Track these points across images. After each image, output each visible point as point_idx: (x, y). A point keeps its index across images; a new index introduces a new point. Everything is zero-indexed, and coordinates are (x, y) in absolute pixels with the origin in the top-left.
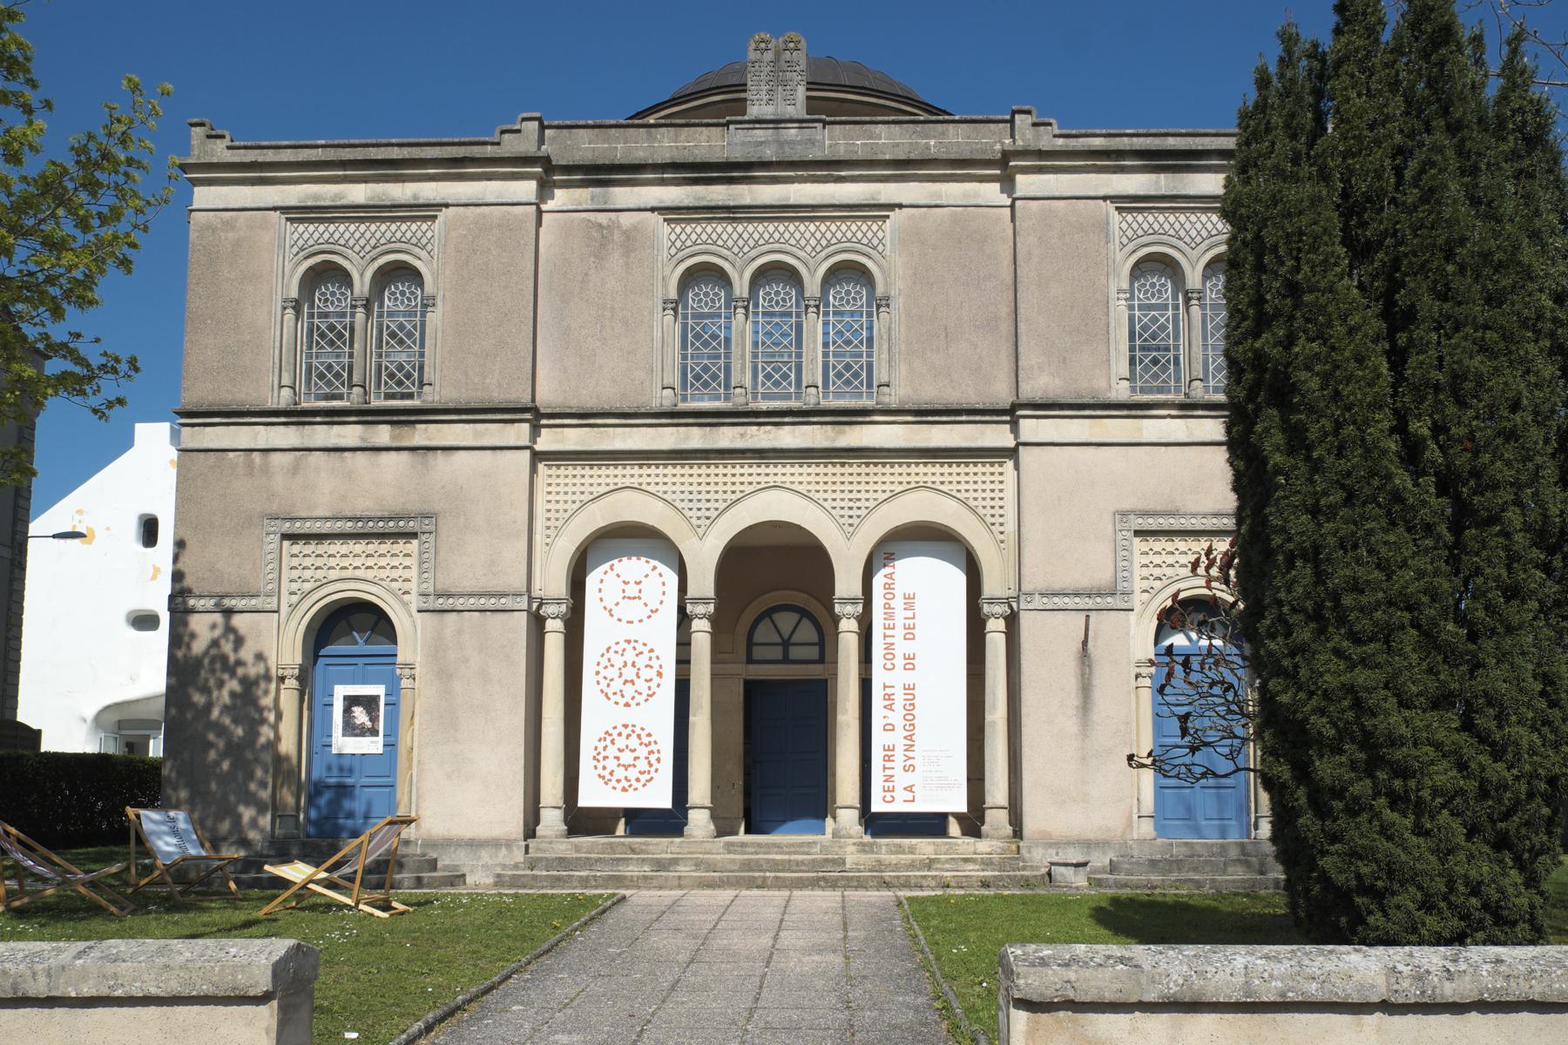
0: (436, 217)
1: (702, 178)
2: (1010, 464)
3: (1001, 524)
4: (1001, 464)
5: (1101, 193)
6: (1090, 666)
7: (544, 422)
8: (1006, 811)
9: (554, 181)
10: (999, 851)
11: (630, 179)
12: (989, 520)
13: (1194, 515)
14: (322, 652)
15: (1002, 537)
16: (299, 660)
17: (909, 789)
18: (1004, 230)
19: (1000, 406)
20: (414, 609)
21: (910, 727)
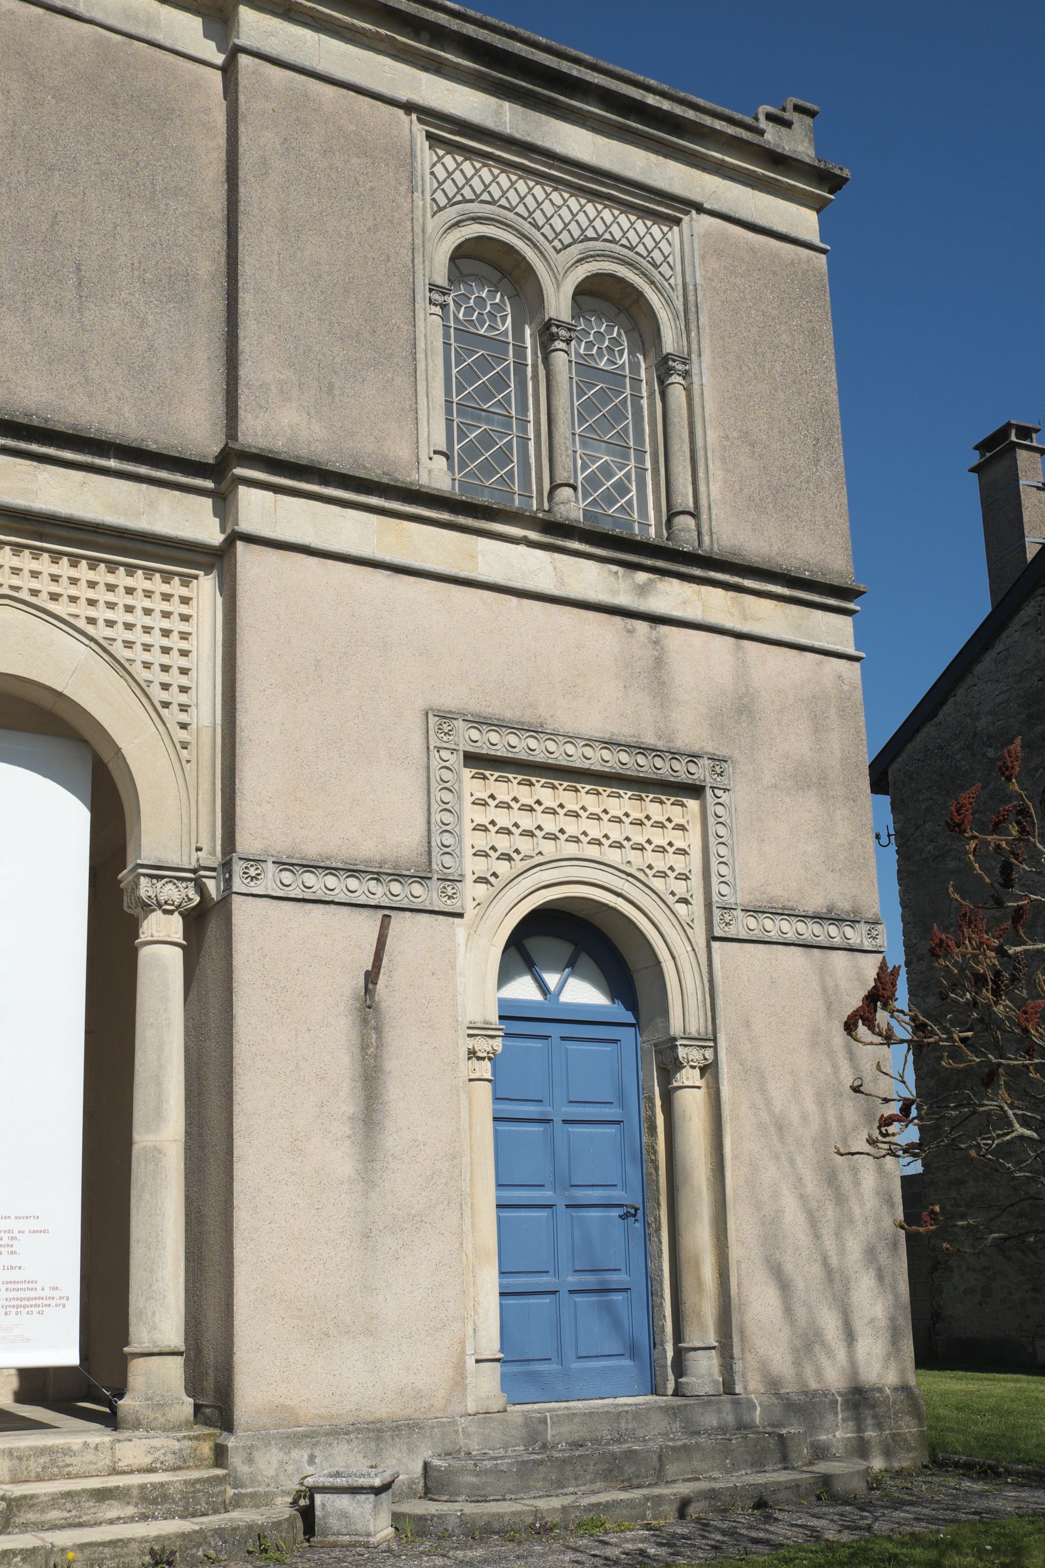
2: (206, 586)
3: (184, 708)
4: (186, 580)
5: (403, 95)
6: (378, 1029)
8: (180, 1360)
10: (171, 1460)
12: (158, 695)
13: (571, 738)
15: (183, 735)
18: (207, 111)
19: (192, 453)
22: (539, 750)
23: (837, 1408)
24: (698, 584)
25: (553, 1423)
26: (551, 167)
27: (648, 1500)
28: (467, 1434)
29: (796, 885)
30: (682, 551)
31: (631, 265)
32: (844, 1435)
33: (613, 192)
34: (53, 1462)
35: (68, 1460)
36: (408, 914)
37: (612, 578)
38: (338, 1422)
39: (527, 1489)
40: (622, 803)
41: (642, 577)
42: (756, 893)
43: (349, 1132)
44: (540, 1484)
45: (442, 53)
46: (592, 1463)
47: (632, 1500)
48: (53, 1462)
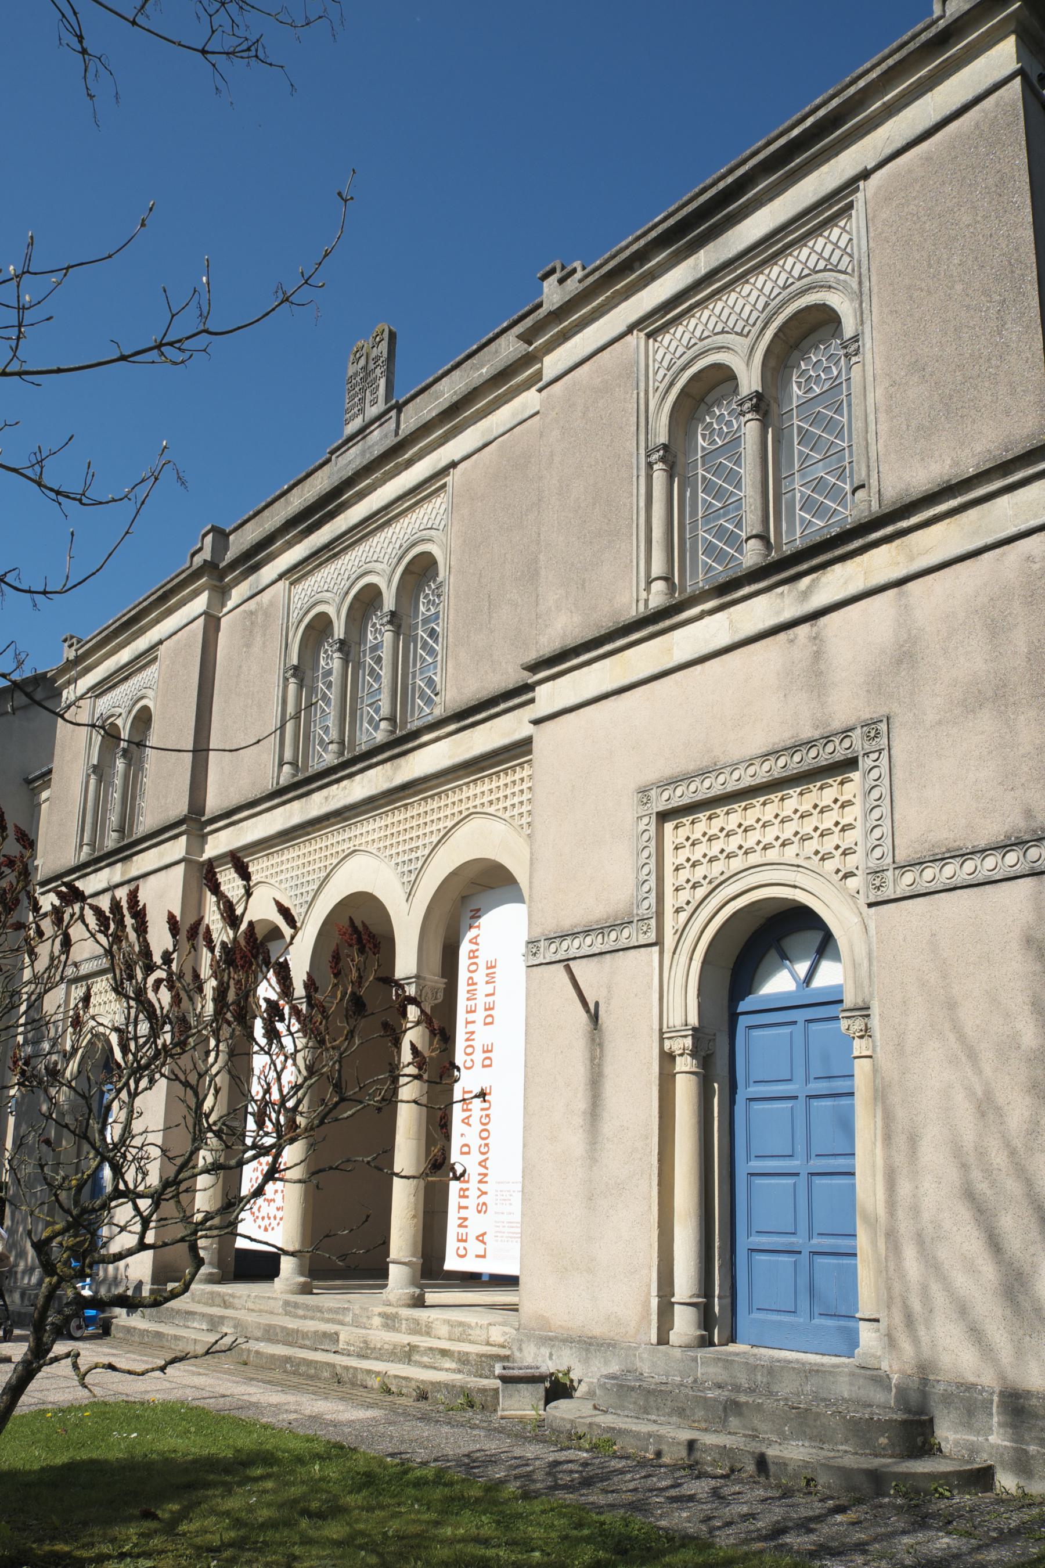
0: (852, 202)
1: (815, 156)
5: (622, 328)
6: (601, 1045)
7: (209, 829)
9: (228, 584)
11: (268, 555)
13: (734, 766)
14: (742, 1007)
16: (693, 1020)
17: (481, 1238)
20: (862, 901)
21: (485, 1149)
22: (714, 786)
23: (991, 1408)
24: (861, 554)
25: (702, 1363)
26: (736, 269)
27: (650, 1436)
28: (641, 1359)
29: (964, 821)
30: (831, 537)
31: (810, 289)
32: (999, 1442)
33: (826, 215)
34: (464, 1331)
35: (470, 1332)
36: (621, 953)
37: (778, 601)
38: (571, 1333)
39: (623, 1408)
40: (794, 801)
41: (806, 581)
42: (916, 845)
43: (582, 1123)
44: (631, 1406)
45: (646, 267)
46: (669, 1399)
47: (639, 1433)
48: (464, 1331)
